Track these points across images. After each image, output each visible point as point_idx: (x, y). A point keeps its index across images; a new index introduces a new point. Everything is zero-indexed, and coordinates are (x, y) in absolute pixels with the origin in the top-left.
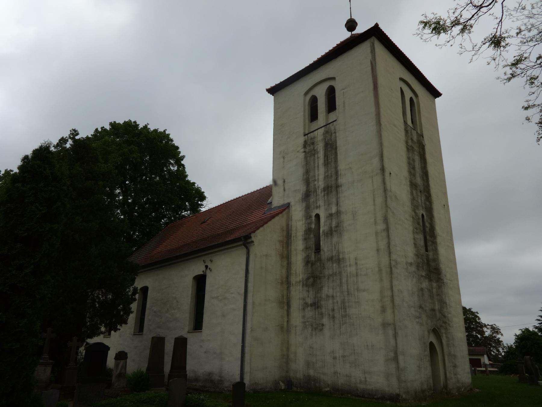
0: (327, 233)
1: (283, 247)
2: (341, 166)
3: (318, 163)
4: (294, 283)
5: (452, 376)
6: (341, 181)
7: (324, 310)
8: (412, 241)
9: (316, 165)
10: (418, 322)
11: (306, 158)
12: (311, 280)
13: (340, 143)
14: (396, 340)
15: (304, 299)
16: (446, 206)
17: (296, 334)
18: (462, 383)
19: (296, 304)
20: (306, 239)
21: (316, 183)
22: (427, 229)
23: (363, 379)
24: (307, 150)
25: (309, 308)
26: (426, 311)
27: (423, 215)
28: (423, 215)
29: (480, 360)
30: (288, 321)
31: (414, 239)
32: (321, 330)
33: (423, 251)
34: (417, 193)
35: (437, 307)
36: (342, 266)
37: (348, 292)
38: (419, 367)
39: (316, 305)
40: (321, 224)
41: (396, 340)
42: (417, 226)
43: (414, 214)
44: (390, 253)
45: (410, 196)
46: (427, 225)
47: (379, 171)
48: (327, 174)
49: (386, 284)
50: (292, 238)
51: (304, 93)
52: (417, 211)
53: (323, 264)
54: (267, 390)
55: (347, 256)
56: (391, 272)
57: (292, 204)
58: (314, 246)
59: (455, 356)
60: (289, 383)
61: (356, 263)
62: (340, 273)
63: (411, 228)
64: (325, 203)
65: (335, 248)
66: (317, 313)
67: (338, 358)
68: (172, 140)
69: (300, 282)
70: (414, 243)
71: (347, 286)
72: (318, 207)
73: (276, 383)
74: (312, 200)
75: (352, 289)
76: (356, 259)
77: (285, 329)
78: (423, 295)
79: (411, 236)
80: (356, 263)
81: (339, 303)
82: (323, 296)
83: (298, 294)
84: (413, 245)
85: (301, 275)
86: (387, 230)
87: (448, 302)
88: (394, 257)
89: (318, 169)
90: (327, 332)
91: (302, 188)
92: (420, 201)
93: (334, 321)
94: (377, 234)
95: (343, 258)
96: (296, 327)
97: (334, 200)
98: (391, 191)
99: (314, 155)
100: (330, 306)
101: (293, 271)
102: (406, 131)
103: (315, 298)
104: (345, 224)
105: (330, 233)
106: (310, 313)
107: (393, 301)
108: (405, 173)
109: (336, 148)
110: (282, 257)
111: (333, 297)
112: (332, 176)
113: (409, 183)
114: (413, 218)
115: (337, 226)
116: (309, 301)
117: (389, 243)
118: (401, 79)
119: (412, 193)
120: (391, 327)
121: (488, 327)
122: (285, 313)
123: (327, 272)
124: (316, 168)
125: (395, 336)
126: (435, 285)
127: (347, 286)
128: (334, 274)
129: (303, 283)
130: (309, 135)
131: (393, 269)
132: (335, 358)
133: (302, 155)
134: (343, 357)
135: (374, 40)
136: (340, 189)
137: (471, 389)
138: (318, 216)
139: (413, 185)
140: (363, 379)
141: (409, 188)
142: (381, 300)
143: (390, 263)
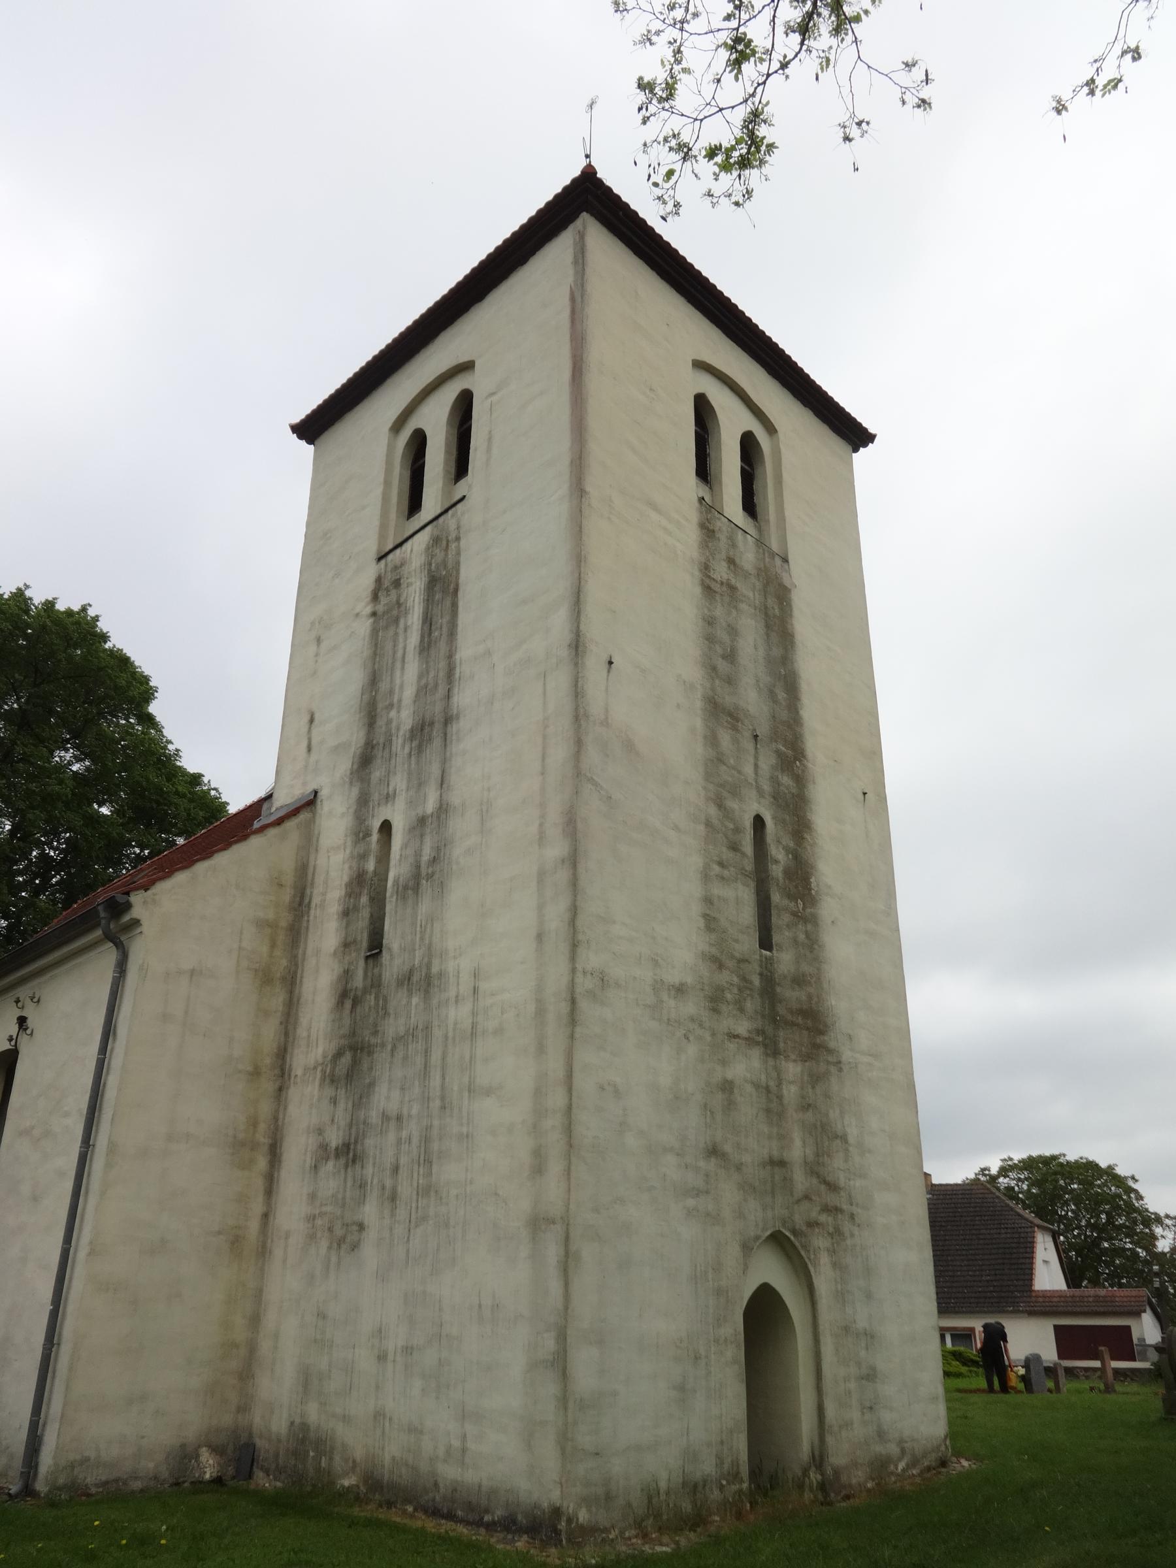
0: (406, 888)
1: (273, 945)
2: (466, 650)
3: (405, 648)
4: (299, 1072)
5: (855, 1415)
6: (463, 698)
7: (369, 1170)
8: (696, 909)
9: (399, 654)
10: (690, 1213)
11: (375, 632)
12: (347, 1059)
13: (468, 573)
14: (566, 1285)
15: (320, 1131)
16: (873, 797)
17: (285, 1261)
18: (901, 1442)
19: (297, 1149)
20: (346, 914)
21: (393, 714)
22: (777, 871)
23: (456, 1443)
24: (380, 608)
25: (331, 1164)
26: (739, 1167)
27: (759, 822)
28: (759, 822)
29: (1128, 1328)
30: (266, 1216)
31: (708, 901)
32: (355, 1247)
33: (748, 944)
34: (735, 741)
35: (798, 1150)
36: (435, 1002)
37: (443, 1098)
38: (681, 1388)
39: (349, 1153)
40: (392, 856)
41: (566, 1285)
42: (727, 855)
43: (713, 811)
44: (574, 946)
45: (699, 749)
46: (778, 854)
47: (565, 653)
48: (424, 681)
49: (555, 1064)
50: (312, 912)
51: (390, 424)
52: (732, 804)
53: (385, 1000)
54: (137, 1485)
55: (451, 966)
56: (573, 1018)
57: (323, 794)
58: (365, 935)
59: (869, 1337)
60: (242, 1455)
61: (475, 990)
62: (428, 1028)
63: (696, 861)
64: (409, 780)
65: (422, 939)
66: (349, 1184)
67: (390, 1357)
68: (104, 637)
69: (315, 1068)
70: (705, 916)
71: (443, 1077)
72: (389, 798)
73: (185, 1456)
74: (377, 774)
75: (456, 1088)
76: (476, 975)
77: (248, 1246)
78: (730, 1105)
79: (694, 889)
80: (475, 990)
81: (415, 1141)
82: (374, 1117)
83: (309, 1111)
84: (701, 923)
85: (321, 1042)
86: (573, 860)
87: (853, 1133)
88: (591, 959)
89: (403, 668)
90: (370, 1253)
91: (355, 737)
92: (749, 770)
93: (393, 1210)
94: (541, 876)
95: (441, 975)
96: (287, 1235)
97: (435, 769)
98: (605, 723)
99: (396, 621)
100: (389, 1157)
101: (302, 1032)
102: (708, 531)
103: (350, 1125)
104: (457, 851)
105: (413, 886)
106: (331, 1181)
107: (569, 1129)
108: (684, 663)
109: (456, 590)
110: (265, 978)
111: (399, 1118)
112: (436, 686)
113: (699, 704)
114: (708, 824)
115: (434, 860)
116: (335, 1139)
117: (574, 910)
118: (701, 366)
119: (712, 740)
120: (558, 1236)
121: (1168, 1222)
122: (259, 1183)
123: (392, 1027)
124: (398, 665)
125: (568, 1264)
126: (793, 1069)
127: (443, 1077)
128: (409, 1035)
129: (324, 1072)
130: (390, 557)
131: (583, 1004)
132: (382, 1358)
133: (364, 627)
134: (408, 1350)
135: (591, 231)
136: (454, 728)
137: (943, 1463)
138: (386, 827)
139: (720, 713)
140: (456, 1443)
141: (699, 723)
142: (535, 1126)
143: (572, 984)
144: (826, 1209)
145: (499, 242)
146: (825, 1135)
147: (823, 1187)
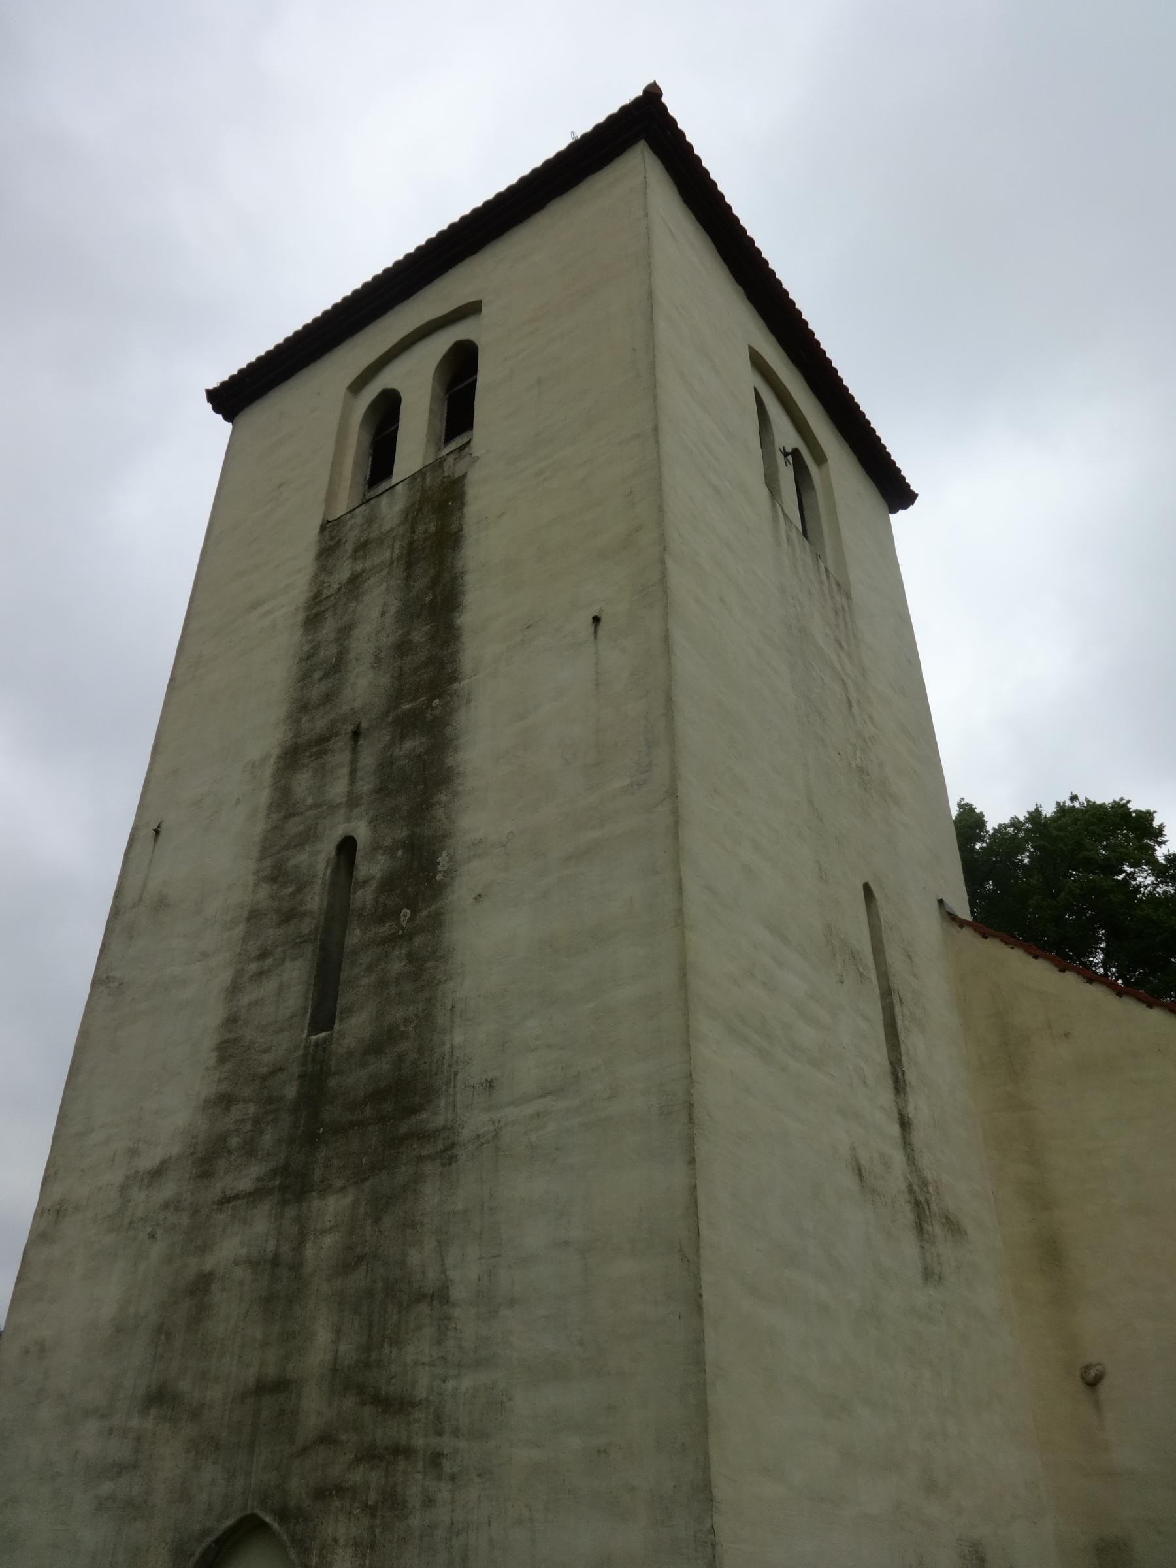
78: (201, 1312)
144: (370, 1455)
145: (538, 163)
146: (391, 1299)
147: (368, 1411)
